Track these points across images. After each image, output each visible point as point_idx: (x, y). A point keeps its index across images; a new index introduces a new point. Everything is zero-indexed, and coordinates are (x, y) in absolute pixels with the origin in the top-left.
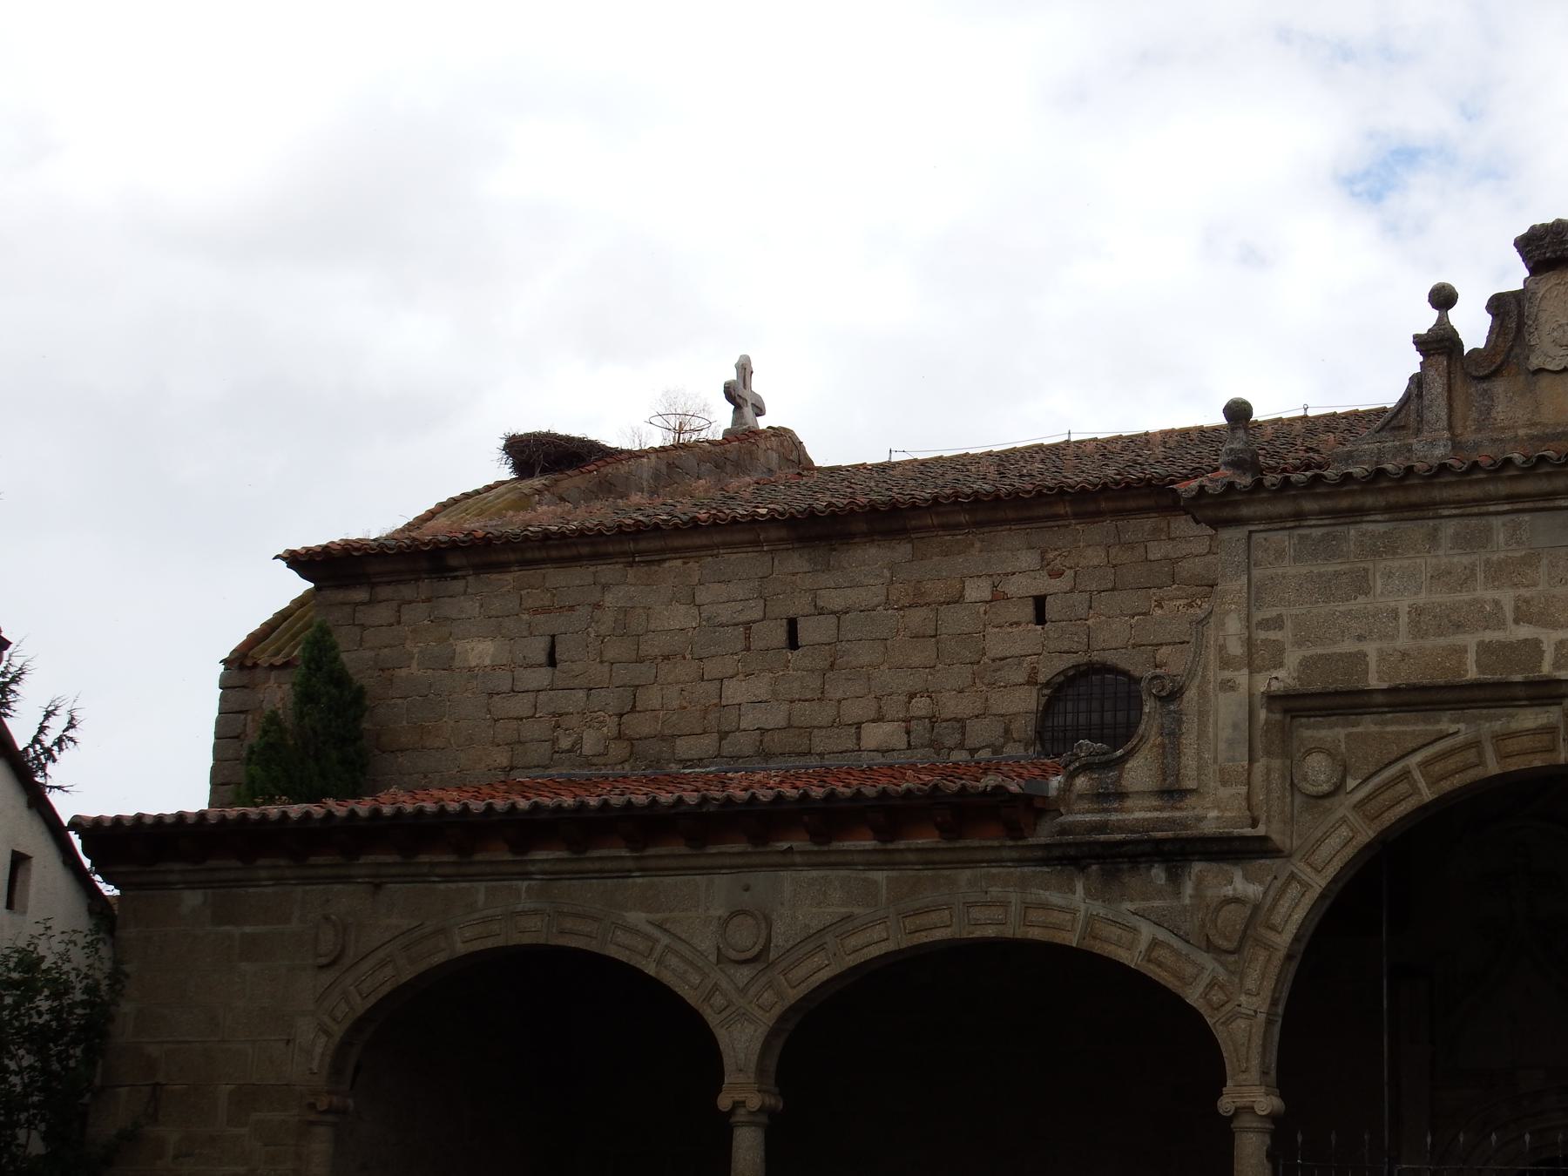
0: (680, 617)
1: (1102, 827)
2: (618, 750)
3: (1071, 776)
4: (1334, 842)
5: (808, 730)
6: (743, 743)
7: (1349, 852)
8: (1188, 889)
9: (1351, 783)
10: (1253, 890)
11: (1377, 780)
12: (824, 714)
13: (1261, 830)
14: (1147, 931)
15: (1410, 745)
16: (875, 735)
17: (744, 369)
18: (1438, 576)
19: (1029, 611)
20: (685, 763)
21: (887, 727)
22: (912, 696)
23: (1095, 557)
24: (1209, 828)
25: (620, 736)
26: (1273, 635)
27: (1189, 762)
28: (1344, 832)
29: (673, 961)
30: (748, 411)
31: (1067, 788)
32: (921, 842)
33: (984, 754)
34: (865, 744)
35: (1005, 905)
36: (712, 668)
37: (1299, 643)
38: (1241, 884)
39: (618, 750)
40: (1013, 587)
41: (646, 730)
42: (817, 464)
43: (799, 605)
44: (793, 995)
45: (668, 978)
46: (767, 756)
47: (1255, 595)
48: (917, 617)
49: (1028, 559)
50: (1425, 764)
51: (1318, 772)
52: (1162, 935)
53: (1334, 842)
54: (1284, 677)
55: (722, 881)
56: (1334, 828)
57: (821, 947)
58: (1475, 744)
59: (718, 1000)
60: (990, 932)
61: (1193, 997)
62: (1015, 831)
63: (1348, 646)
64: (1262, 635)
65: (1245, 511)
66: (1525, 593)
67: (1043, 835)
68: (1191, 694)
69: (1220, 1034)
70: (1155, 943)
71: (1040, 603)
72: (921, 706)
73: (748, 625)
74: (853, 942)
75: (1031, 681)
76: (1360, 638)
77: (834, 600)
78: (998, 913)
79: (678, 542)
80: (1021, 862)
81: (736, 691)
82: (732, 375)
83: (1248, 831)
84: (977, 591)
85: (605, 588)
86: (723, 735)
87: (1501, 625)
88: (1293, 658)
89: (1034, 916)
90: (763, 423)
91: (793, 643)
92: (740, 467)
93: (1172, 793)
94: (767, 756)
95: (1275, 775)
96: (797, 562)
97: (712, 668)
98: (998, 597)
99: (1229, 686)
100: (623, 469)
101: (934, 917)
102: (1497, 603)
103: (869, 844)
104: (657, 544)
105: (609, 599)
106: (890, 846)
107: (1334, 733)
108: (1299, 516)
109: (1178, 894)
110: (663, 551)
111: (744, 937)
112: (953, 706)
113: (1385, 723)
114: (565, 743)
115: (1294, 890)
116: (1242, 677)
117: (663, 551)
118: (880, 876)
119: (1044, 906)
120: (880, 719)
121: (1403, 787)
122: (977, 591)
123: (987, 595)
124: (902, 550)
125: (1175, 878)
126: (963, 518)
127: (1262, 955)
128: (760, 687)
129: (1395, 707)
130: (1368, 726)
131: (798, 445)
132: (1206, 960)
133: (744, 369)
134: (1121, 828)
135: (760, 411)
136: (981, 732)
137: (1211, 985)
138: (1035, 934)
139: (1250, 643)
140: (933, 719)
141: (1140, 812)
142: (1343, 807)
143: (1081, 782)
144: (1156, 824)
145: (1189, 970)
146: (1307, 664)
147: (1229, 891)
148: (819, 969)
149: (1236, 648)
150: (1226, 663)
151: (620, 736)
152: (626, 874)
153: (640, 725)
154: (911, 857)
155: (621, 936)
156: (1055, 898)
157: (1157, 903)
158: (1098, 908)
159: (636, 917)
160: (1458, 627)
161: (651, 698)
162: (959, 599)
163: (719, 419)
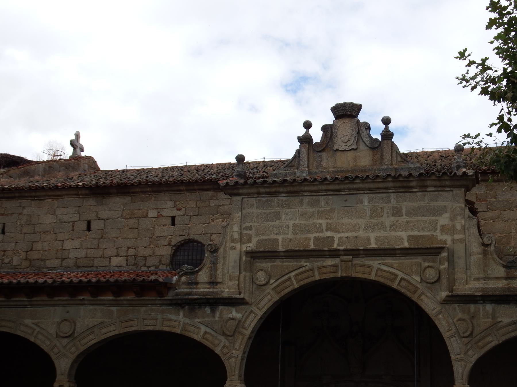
0: (49, 219)
1: (190, 294)
2: (25, 264)
3: (180, 277)
4: (266, 300)
5: (93, 258)
6: (70, 262)
7: (271, 304)
8: (217, 315)
9: (272, 281)
10: (239, 316)
11: (280, 281)
12: (99, 253)
13: (242, 296)
14: (203, 329)
15: (291, 270)
16: (115, 261)
17: (77, 136)
18: (302, 215)
19: (169, 221)
20: (49, 269)
21: (120, 258)
22: (129, 248)
23: (192, 204)
24: (225, 295)
25: (26, 259)
26: (248, 232)
27: (219, 273)
28: (269, 297)
29: (40, 336)
30: (78, 150)
31: (179, 280)
32: (129, 297)
33: (152, 268)
34: (112, 264)
35: (156, 319)
36: (60, 237)
37: (257, 235)
38: (235, 313)
39: (25, 264)
40: (165, 213)
41: (35, 257)
42: (101, 169)
43: (92, 216)
44: (82, 349)
45: (38, 343)
46: (78, 267)
47: (243, 219)
48: (132, 222)
49: (170, 204)
50: (296, 276)
51: (261, 277)
52: (208, 330)
53: (266, 300)
54: (251, 246)
55: (59, 310)
56: (266, 296)
57: (93, 332)
58: (312, 270)
59: (56, 350)
60: (151, 328)
61: (218, 351)
62: (161, 294)
63: (273, 237)
64: (245, 232)
65: (241, 191)
66: (330, 221)
67: (170, 296)
68: (221, 250)
69: (226, 363)
70: (206, 333)
71: (173, 218)
72: (132, 252)
73: (73, 222)
74: (103, 331)
75: (169, 244)
76: (277, 234)
77: (104, 215)
78: (153, 322)
79: (50, 193)
80: (162, 305)
81: (68, 245)
82: (73, 138)
83: (238, 296)
84: (152, 214)
85: (24, 208)
86: (63, 260)
87: (322, 231)
88: (255, 240)
89: (166, 323)
90: (83, 154)
91: (89, 229)
92: (74, 169)
93: (213, 283)
94: (78, 267)
95: (247, 278)
96: (91, 202)
97: (60, 237)
98: (159, 216)
99: (233, 248)
100: (33, 167)
101: (132, 323)
102: (320, 224)
103: (111, 298)
104: (43, 194)
105: (25, 212)
106: (118, 299)
107: (267, 265)
108: (259, 194)
109: (214, 316)
110: (44, 196)
111: (66, 328)
112: (143, 252)
113: (283, 262)
114: (6, 261)
115: (252, 316)
116: (238, 245)
117: (44, 196)
118: (114, 309)
119: (170, 320)
120: (117, 256)
121: (288, 283)
122: (152, 214)
123: (156, 215)
124: (128, 199)
125: (213, 311)
126: (149, 189)
127: (241, 337)
128: (77, 243)
129: (287, 257)
130: (278, 263)
131: (95, 162)
132: (222, 338)
133: (77, 136)
134: (196, 294)
135: (82, 150)
136: (151, 261)
137: (224, 347)
138: (166, 329)
139: (241, 234)
140: (135, 256)
141: (202, 289)
142: (269, 289)
143: (184, 279)
144: (208, 293)
145: (217, 342)
146: (259, 242)
147: (231, 316)
148: (92, 340)
149: (236, 236)
150: (233, 241)
151: (26, 259)
152: (25, 306)
153: (34, 255)
154: (125, 302)
155: (22, 328)
156: (173, 317)
157: (207, 319)
158: (187, 321)
159: (28, 321)
160: (308, 231)
161: (38, 246)
162: (146, 216)
163: (68, 152)
